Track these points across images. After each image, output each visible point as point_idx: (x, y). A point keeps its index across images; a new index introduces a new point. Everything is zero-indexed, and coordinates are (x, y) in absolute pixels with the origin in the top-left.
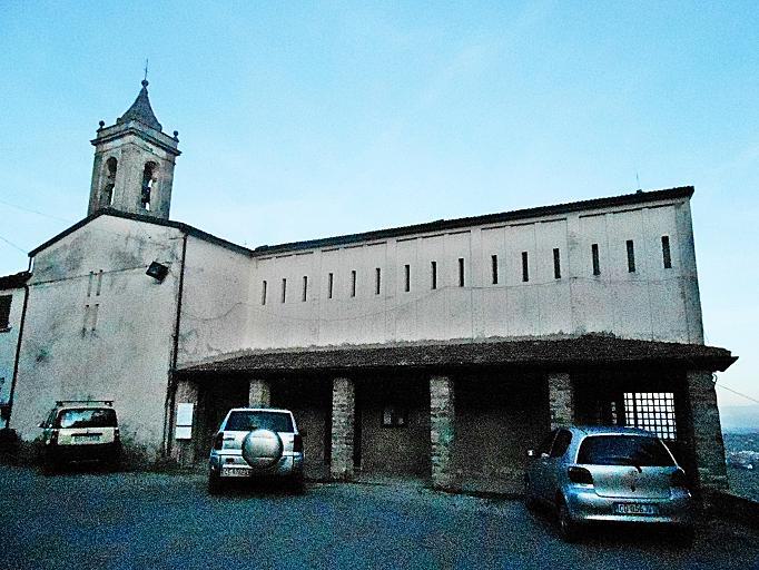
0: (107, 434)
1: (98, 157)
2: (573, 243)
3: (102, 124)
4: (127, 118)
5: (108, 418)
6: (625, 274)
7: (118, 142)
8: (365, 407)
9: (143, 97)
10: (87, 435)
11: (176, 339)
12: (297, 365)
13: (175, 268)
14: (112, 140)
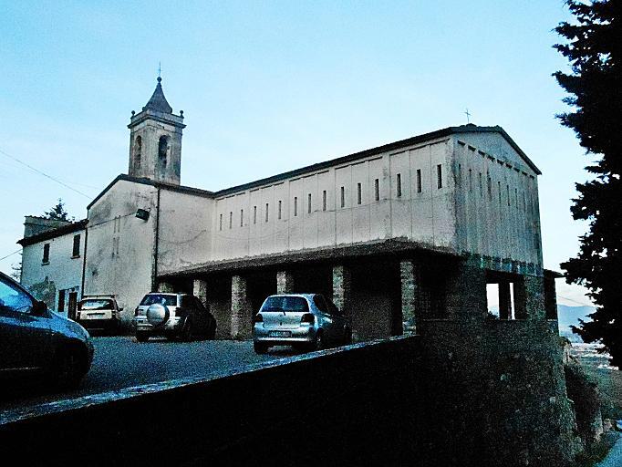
0: (108, 314)
1: (132, 137)
2: (387, 175)
3: (133, 112)
4: (151, 105)
5: (111, 305)
6: (415, 195)
7: (142, 125)
8: (355, 288)
9: (159, 88)
10: (96, 314)
11: (156, 256)
12: (268, 263)
13: (153, 212)
14: (139, 124)
